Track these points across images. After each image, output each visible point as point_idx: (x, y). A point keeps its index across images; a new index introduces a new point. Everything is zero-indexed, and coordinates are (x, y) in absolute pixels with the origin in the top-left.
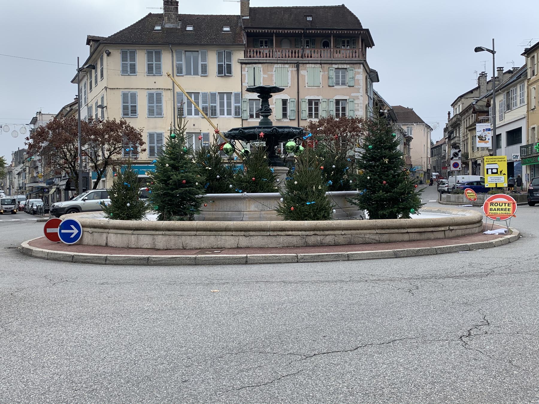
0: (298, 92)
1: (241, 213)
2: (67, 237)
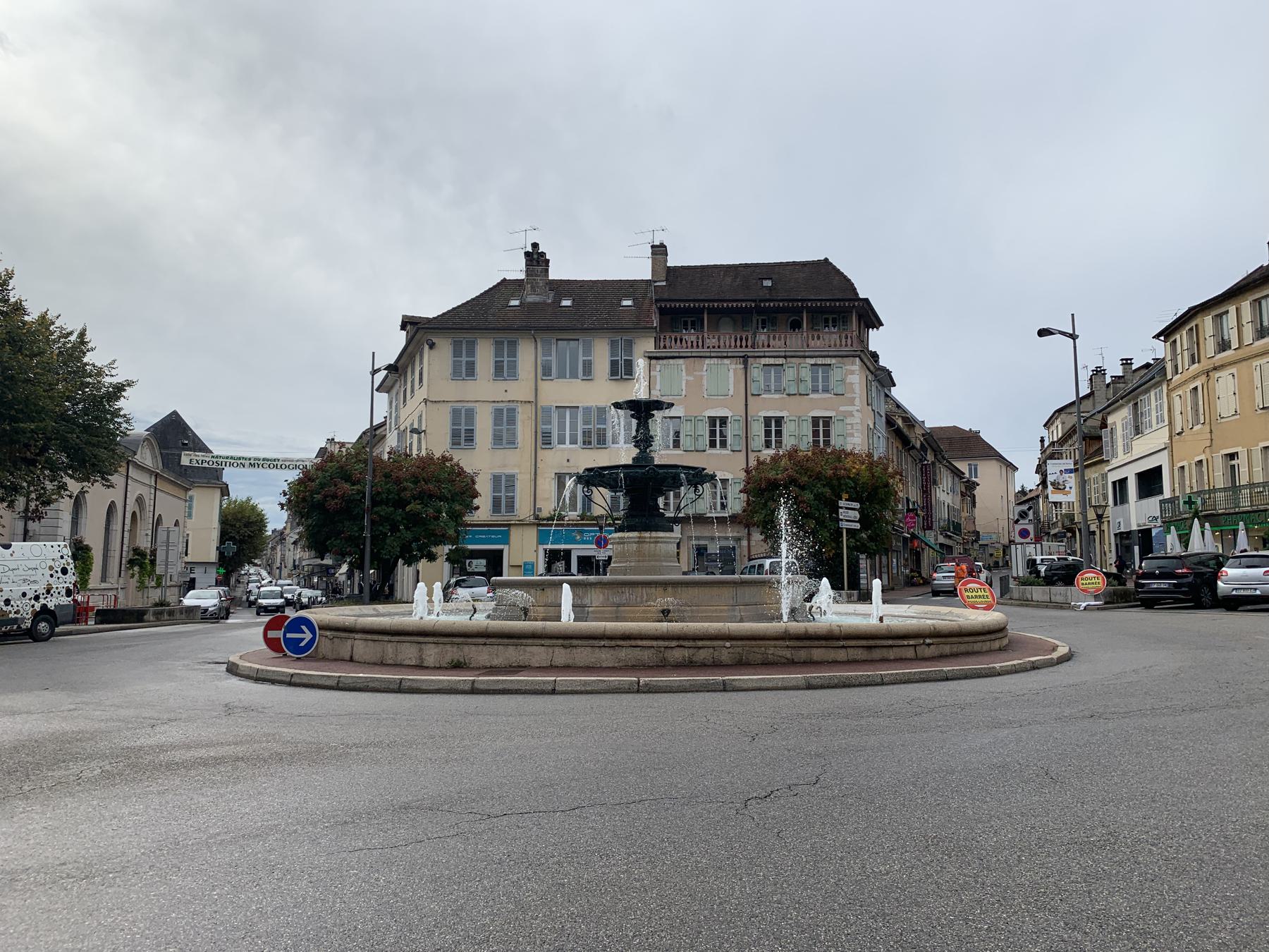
0: (746, 405)
1: (584, 610)
2: (295, 646)
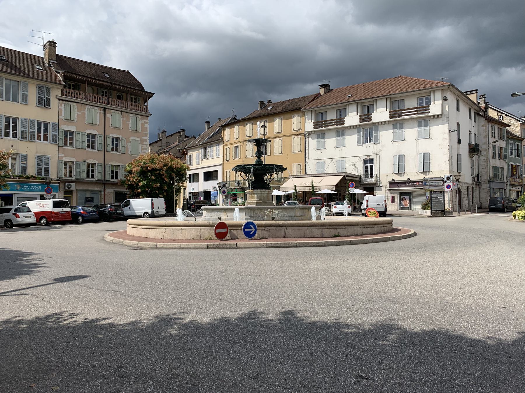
0: (105, 130)
